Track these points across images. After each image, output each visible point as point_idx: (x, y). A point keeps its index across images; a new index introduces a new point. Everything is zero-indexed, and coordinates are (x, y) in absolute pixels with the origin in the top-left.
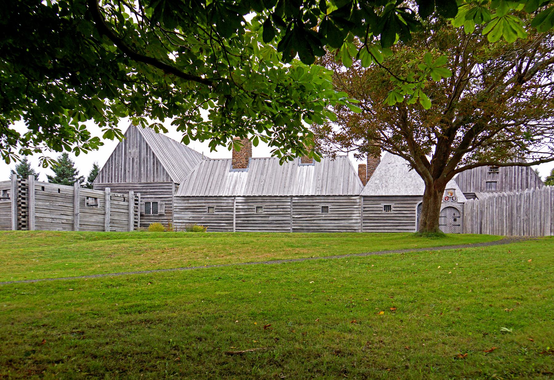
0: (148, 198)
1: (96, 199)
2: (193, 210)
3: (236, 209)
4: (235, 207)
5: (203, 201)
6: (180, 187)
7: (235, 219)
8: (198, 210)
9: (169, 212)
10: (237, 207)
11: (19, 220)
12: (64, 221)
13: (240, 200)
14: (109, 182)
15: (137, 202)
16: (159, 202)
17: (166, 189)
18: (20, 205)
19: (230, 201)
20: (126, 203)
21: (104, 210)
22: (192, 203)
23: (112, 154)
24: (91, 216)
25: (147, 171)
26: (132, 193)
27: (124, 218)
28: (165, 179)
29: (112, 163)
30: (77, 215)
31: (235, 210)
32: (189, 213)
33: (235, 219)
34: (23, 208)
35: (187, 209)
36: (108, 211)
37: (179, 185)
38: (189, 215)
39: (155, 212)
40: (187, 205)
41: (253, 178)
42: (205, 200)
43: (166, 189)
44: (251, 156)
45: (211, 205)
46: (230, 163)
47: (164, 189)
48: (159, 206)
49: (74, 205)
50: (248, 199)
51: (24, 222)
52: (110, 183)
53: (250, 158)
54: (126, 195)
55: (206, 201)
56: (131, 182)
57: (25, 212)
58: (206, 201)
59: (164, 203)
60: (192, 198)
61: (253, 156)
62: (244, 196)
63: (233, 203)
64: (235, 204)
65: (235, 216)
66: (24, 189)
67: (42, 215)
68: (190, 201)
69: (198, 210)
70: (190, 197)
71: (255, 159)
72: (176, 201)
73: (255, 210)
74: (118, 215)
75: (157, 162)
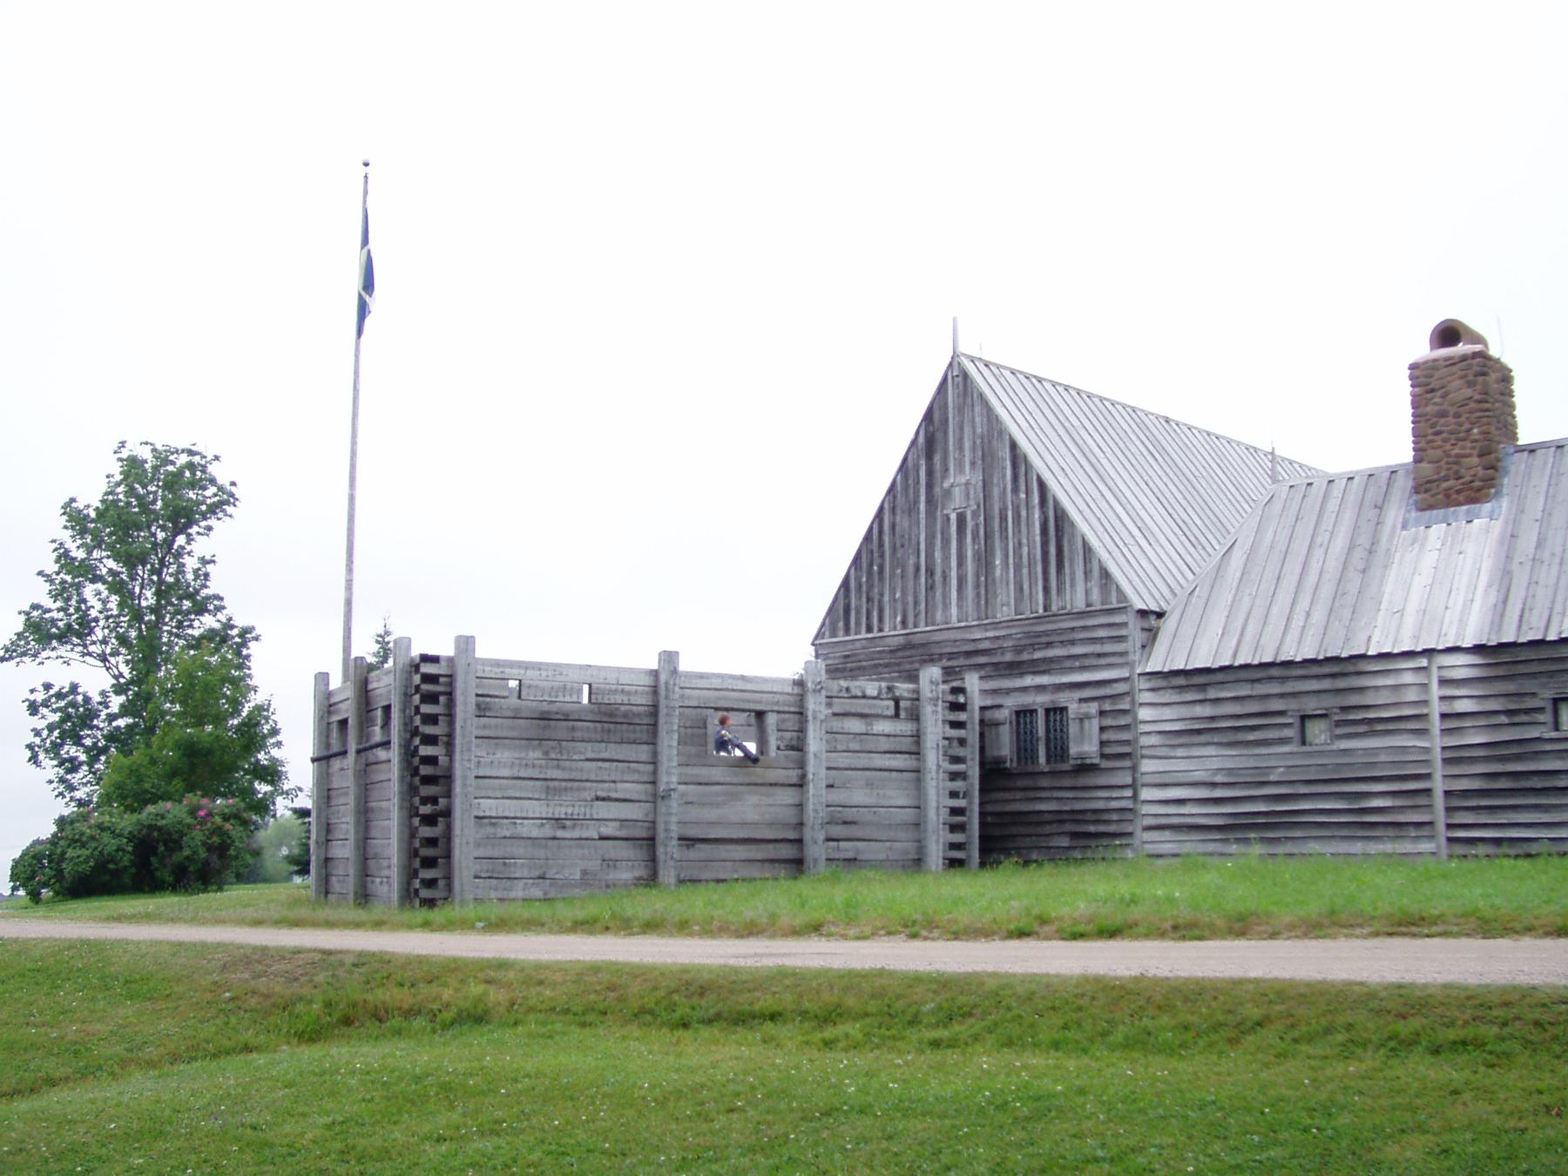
0: (1024, 689)
1: (760, 715)
2: (1232, 733)
3: (1444, 716)
4: (1436, 708)
5: (1275, 688)
6: (1168, 626)
7: (1438, 771)
8: (1252, 736)
9: (1119, 753)
10: (1446, 709)
11: (413, 833)
12: (608, 830)
13: (1461, 666)
14: (869, 630)
15: (962, 716)
16: (1073, 709)
17: (1101, 640)
18: (416, 772)
19: (1408, 678)
20: (904, 727)
21: (802, 765)
22: (1229, 704)
23: (881, 509)
24: (734, 797)
25: (1018, 567)
26: (931, 674)
27: (897, 796)
28: (1095, 595)
29: (881, 545)
30: (666, 797)
31: (1436, 724)
32: (1211, 751)
33: (1438, 771)
34: (428, 780)
35: (1199, 732)
36: (816, 770)
37: (1160, 615)
38: (1210, 761)
39: (1058, 749)
40: (1200, 711)
41: (1527, 543)
42: (1283, 679)
43: (1101, 640)
44: (1514, 437)
45: (1311, 705)
46: (1404, 484)
47: (1093, 640)
48: (1073, 729)
49: (655, 754)
50: (1500, 658)
51: (432, 842)
52: (875, 634)
53: (1504, 448)
54: (903, 688)
55: (1290, 687)
56: (954, 622)
57: (434, 800)
58: (1290, 687)
59: (1093, 708)
60: (1220, 677)
61: (1525, 436)
62: (1478, 649)
63: (1425, 687)
64: (1436, 691)
65: (1438, 755)
66: (431, 698)
67: (510, 807)
68: (1212, 694)
69: (1252, 736)
70: (1207, 671)
71: (1531, 449)
72: (1147, 697)
73: (1546, 717)
74: (870, 785)
75: (1057, 525)
